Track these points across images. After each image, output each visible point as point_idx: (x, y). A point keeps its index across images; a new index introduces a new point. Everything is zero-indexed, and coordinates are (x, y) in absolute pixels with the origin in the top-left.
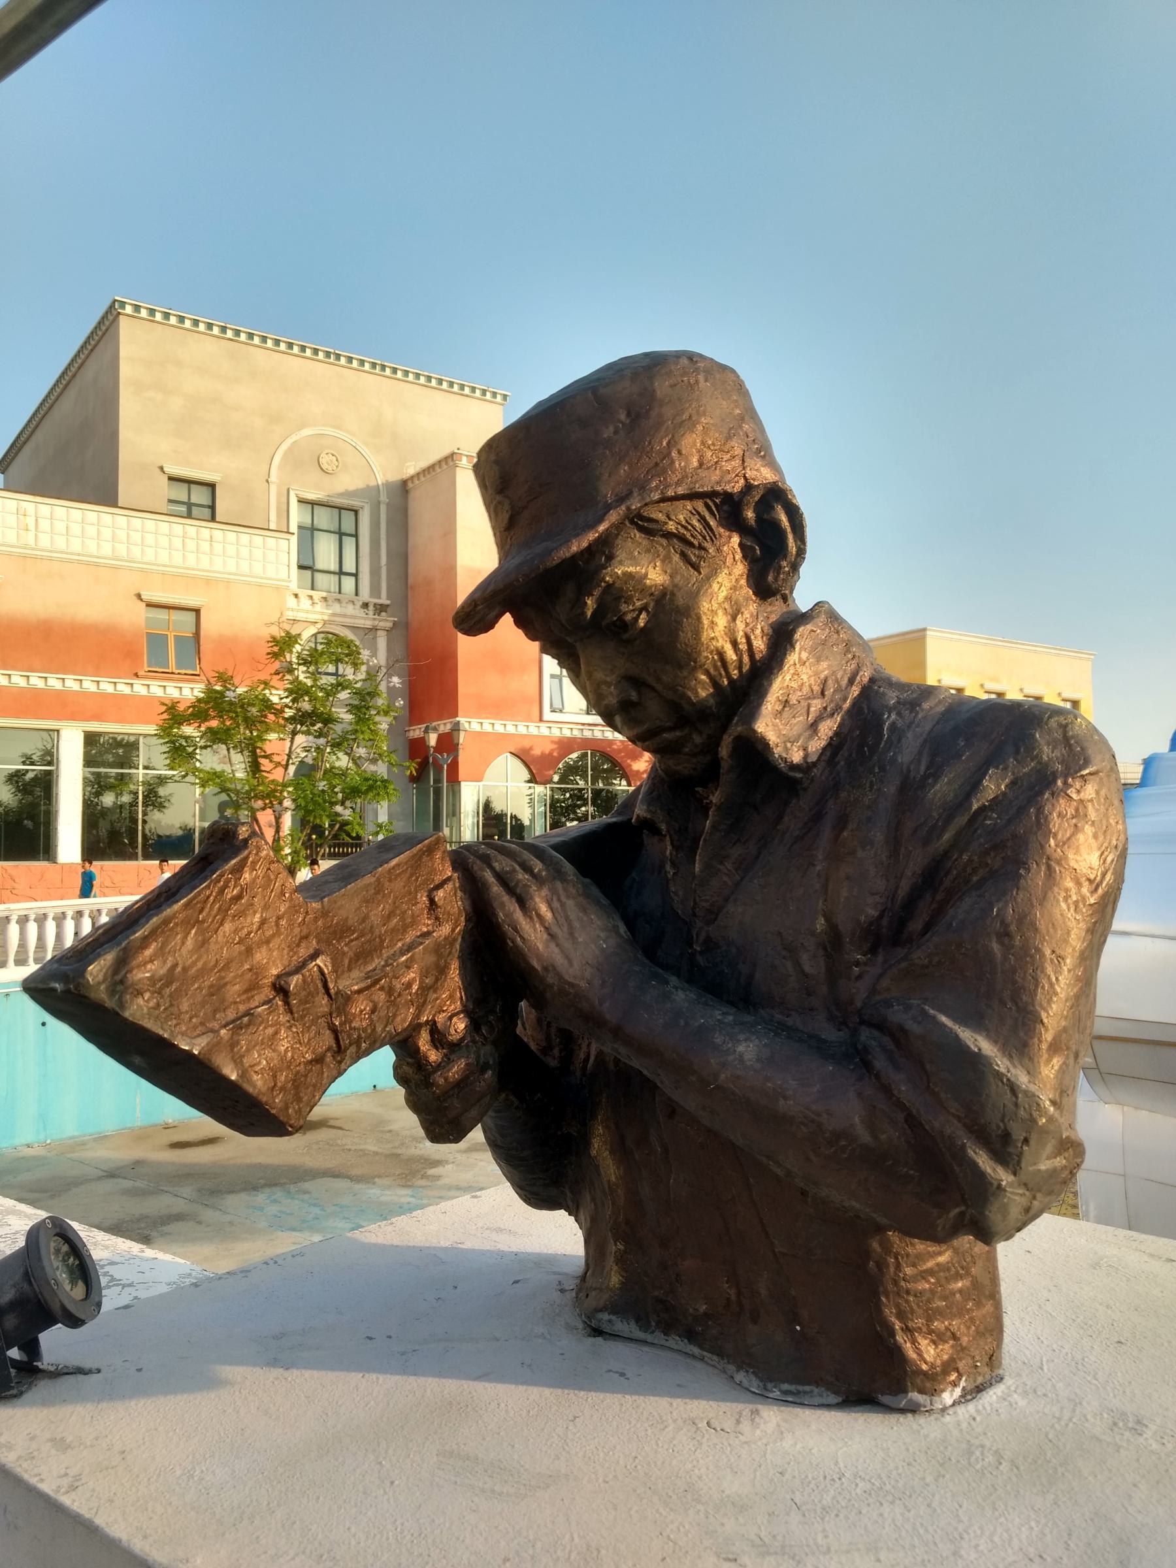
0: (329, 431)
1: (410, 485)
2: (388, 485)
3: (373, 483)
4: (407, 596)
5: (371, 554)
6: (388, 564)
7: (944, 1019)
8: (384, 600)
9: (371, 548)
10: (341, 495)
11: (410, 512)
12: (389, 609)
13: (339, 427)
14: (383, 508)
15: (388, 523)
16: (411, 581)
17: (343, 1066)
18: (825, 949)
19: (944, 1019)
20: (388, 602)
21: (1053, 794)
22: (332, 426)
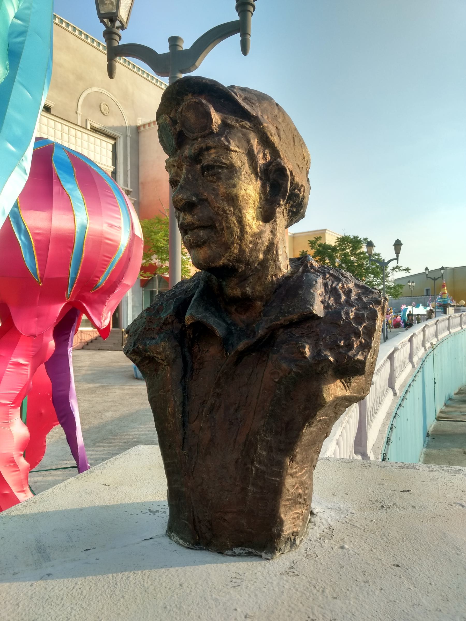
0: (104, 91)
1: (142, 129)
2: (130, 127)
3: (124, 125)
4: (138, 188)
5: (124, 163)
6: (130, 170)
7: (84, 304)
8: (129, 189)
9: (124, 160)
10: (110, 128)
11: (141, 149)
12: (131, 194)
13: (109, 91)
14: (129, 139)
15: (130, 147)
16: (141, 180)
17: (314, 464)
18: (192, 375)
19: (84, 304)
20: (131, 190)
21: (310, 425)
22: (106, 89)
